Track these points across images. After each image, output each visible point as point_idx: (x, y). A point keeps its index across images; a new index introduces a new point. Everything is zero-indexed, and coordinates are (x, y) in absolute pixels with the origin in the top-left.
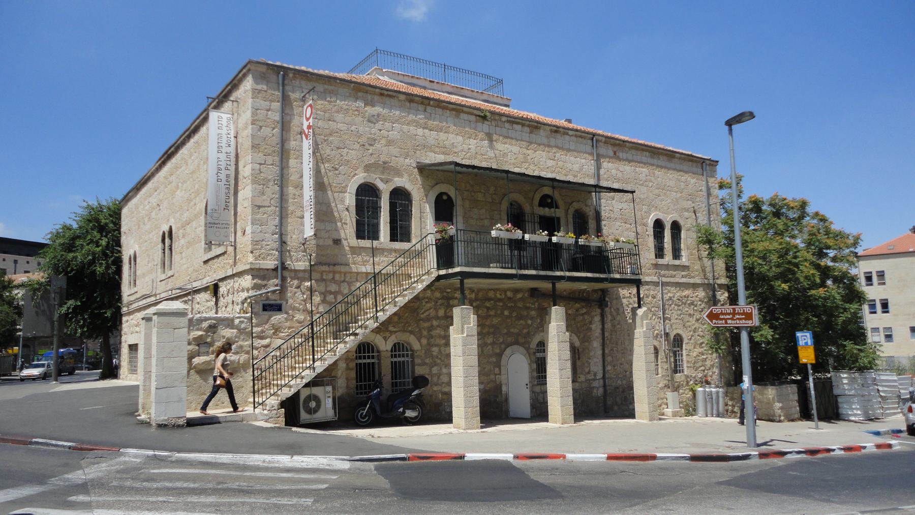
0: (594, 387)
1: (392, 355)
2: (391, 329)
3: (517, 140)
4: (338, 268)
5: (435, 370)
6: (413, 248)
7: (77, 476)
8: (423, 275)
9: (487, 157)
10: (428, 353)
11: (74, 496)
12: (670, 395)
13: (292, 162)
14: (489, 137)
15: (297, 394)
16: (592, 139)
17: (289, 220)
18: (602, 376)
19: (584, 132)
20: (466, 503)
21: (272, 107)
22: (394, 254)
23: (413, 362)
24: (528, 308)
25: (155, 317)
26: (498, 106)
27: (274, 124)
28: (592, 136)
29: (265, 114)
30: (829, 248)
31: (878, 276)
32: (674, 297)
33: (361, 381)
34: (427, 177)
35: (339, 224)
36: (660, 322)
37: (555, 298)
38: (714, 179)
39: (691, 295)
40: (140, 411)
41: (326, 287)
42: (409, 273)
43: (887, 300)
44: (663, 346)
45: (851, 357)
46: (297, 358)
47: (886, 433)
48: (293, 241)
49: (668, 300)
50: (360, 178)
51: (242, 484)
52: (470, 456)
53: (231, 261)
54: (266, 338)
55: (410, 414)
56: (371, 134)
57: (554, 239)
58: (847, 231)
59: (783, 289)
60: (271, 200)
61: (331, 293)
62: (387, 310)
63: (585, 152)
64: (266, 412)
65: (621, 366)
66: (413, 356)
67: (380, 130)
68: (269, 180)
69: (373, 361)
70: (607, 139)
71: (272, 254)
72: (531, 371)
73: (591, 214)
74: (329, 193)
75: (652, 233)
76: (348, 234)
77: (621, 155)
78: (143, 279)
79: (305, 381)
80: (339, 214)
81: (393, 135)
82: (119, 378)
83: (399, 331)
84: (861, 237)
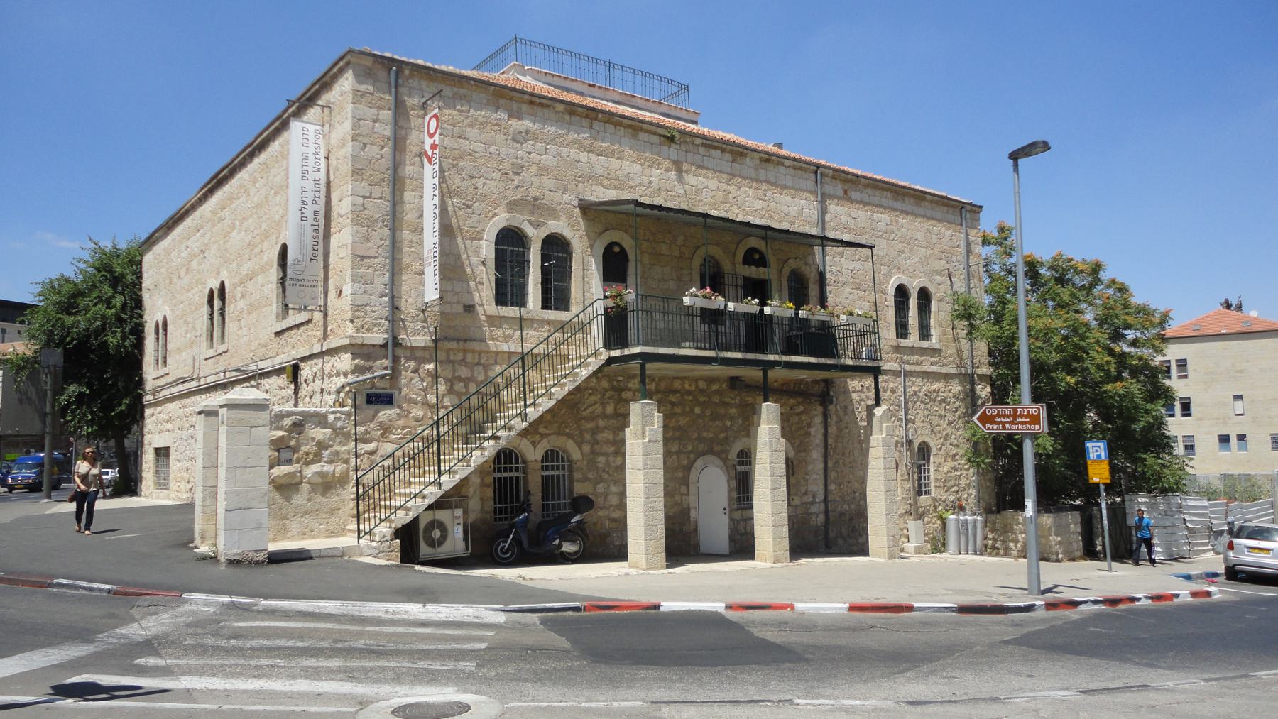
0: (811, 514)
1: (542, 466)
2: (542, 430)
3: (715, 171)
4: (470, 345)
5: (601, 488)
6: (576, 319)
7: (135, 631)
8: (589, 357)
9: (674, 194)
10: (592, 463)
11: (140, 658)
12: (912, 524)
13: (408, 195)
14: (677, 165)
15: (415, 521)
16: (816, 173)
17: (404, 277)
18: (823, 498)
19: (805, 162)
20: (680, 668)
21: (380, 117)
22: (547, 327)
23: (571, 477)
24: (725, 404)
25: (223, 411)
26: (682, 123)
27: (383, 141)
28: (815, 168)
29: (371, 126)
30: (1129, 327)
31: (1178, 366)
32: (920, 392)
33: (500, 503)
34: (593, 220)
35: (472, 284)
36: (900, 426)
37: (767, 391)
38: (976, 231)
39: (943, 389)
40: (197, 542)
41: (454, 371)
42: (566, 353)
43: (1189, 398)
44: (906, 457)
45: (1152, 475)
46: (412, 470)
47: (1199, 577)
48: (409, 306)
49: (912, 395)
50: (502, 219)
51: (368, 642)
52: (668, 606)
53: (319, 333)
54: (371, 442)
55: (568, 548)
56: (517, 158)
57: (767, 310)
58: (1153, 307)
59: (1068, 383)
60: (378, 247)
61: (460, 379)
62: (540, 405)
63: (806, 191)
64: (374, 544)
65: (849, 485)
66: (570, 469)
67: (530, 153)
68: (376, 221)
69: (516, 474)
70: (836, 173)
71: (379, 324)
72: (730, 491)
73: (813, 276)
74: (459, 239)
75: (893, 304)
76: (484, 299)
77: (853, 195)
78: (177, 356)
79: (427, 502)
80: (472, 269)
81: (548, 160)
82: (140, 496)
83: (553, 434)
84: (1171, 315)
